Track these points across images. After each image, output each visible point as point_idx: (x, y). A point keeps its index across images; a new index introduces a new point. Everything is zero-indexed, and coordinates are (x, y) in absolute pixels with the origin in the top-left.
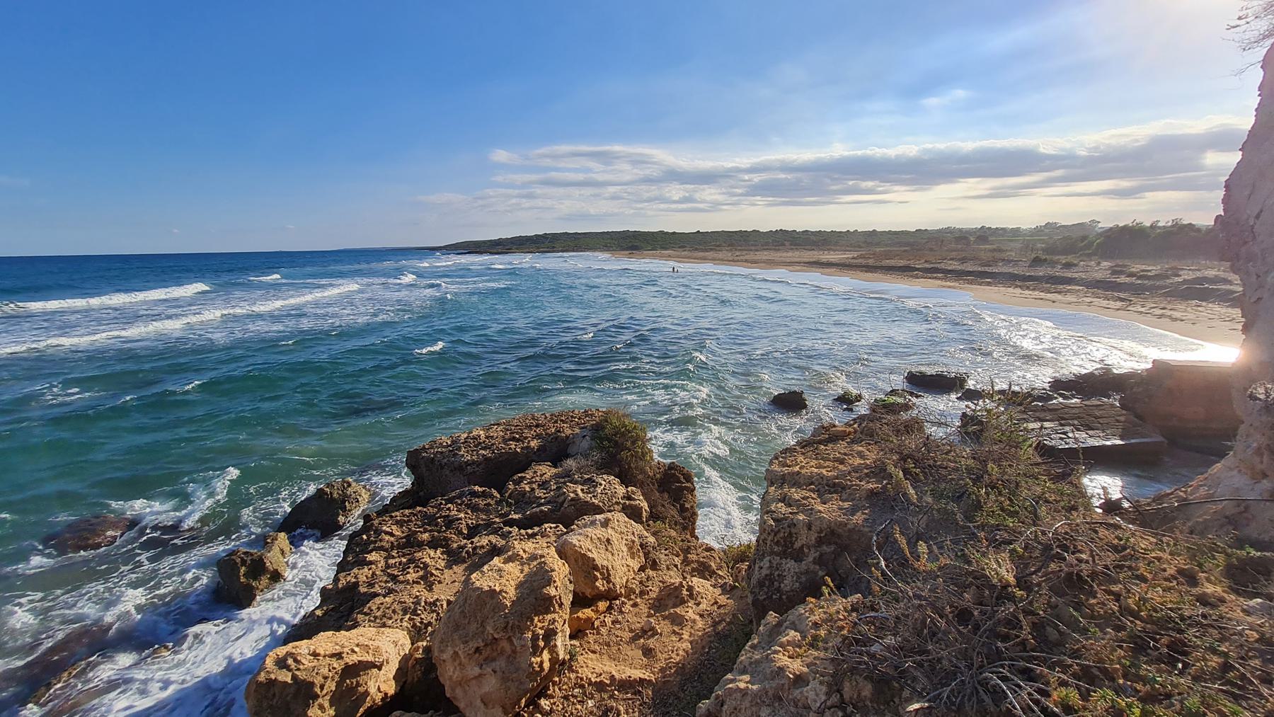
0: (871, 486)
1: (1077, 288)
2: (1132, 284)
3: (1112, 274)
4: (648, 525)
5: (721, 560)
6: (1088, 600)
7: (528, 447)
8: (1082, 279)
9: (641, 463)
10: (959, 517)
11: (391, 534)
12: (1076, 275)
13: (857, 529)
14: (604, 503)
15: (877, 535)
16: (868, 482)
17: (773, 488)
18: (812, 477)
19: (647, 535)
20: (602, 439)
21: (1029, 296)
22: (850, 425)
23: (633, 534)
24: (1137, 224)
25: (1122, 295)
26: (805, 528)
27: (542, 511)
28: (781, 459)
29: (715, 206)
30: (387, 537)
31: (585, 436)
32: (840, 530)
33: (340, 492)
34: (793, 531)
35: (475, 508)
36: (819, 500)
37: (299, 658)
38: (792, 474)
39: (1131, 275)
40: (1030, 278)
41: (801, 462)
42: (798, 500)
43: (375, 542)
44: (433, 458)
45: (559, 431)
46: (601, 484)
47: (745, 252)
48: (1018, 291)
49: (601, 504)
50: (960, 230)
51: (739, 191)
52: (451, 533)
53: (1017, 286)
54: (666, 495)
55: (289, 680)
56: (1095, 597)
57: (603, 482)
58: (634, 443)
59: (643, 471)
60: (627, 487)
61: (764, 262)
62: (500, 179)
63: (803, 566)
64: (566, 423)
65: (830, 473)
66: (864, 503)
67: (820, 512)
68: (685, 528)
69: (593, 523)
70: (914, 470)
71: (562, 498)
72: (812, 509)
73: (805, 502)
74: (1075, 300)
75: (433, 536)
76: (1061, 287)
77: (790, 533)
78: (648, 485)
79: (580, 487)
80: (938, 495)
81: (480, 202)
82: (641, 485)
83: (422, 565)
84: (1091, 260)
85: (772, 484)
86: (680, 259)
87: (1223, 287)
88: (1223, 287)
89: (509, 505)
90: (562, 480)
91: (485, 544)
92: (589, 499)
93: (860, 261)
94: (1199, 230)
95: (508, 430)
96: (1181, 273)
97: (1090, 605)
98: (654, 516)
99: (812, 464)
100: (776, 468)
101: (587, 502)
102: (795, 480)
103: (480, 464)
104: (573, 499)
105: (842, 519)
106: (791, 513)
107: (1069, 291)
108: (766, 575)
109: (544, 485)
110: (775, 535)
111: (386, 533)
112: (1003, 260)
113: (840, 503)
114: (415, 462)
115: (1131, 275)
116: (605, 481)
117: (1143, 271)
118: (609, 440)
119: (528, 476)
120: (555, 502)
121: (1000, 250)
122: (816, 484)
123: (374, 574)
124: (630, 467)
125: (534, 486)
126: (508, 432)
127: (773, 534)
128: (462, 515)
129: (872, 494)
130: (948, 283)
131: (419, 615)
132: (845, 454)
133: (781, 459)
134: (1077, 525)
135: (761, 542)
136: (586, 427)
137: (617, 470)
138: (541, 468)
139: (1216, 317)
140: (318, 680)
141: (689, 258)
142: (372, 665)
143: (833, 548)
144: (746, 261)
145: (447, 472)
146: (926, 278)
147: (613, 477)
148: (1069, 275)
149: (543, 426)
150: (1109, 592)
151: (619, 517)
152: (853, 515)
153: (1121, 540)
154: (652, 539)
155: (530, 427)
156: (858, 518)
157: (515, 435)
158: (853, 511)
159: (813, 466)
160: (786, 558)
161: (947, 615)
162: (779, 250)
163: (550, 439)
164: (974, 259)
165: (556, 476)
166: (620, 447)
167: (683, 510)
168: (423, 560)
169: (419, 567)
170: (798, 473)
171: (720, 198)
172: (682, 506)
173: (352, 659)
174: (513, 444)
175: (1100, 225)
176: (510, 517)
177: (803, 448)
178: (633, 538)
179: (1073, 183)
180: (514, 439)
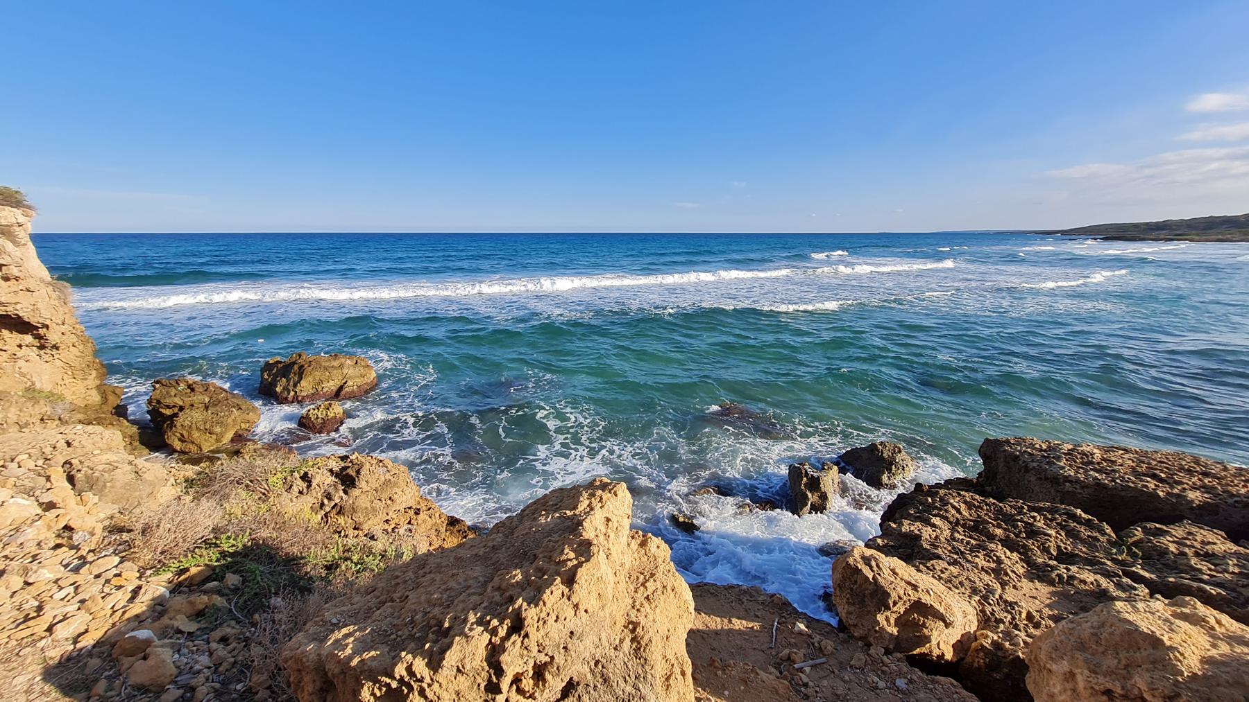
11: (958, 511)
30: (953, 512)
33: (890, 454)
35: (1071, 534)
37: (881, 565)
43: (940, 509)
44: (1018, 456)
52: (1033, 544)
55: (871, 578)
62: (1196, 135)
75: (1008, 536)
81: (1147, 172)
83: (995, 558)
89: (1134, 555)
91: (1088, 580)
103: (1087, 487)
111: (954, 507)
114: (990, 450)
123: (937, 537)
128: (1052, 532)
131: (990, 604)
140: (894, 595)
142: (942, 619)
145: (1033, 479)
168: (998, 554)
169: (991, 557)
173: (926, 599)
174: (1152, 484)
176: (1134, 569)
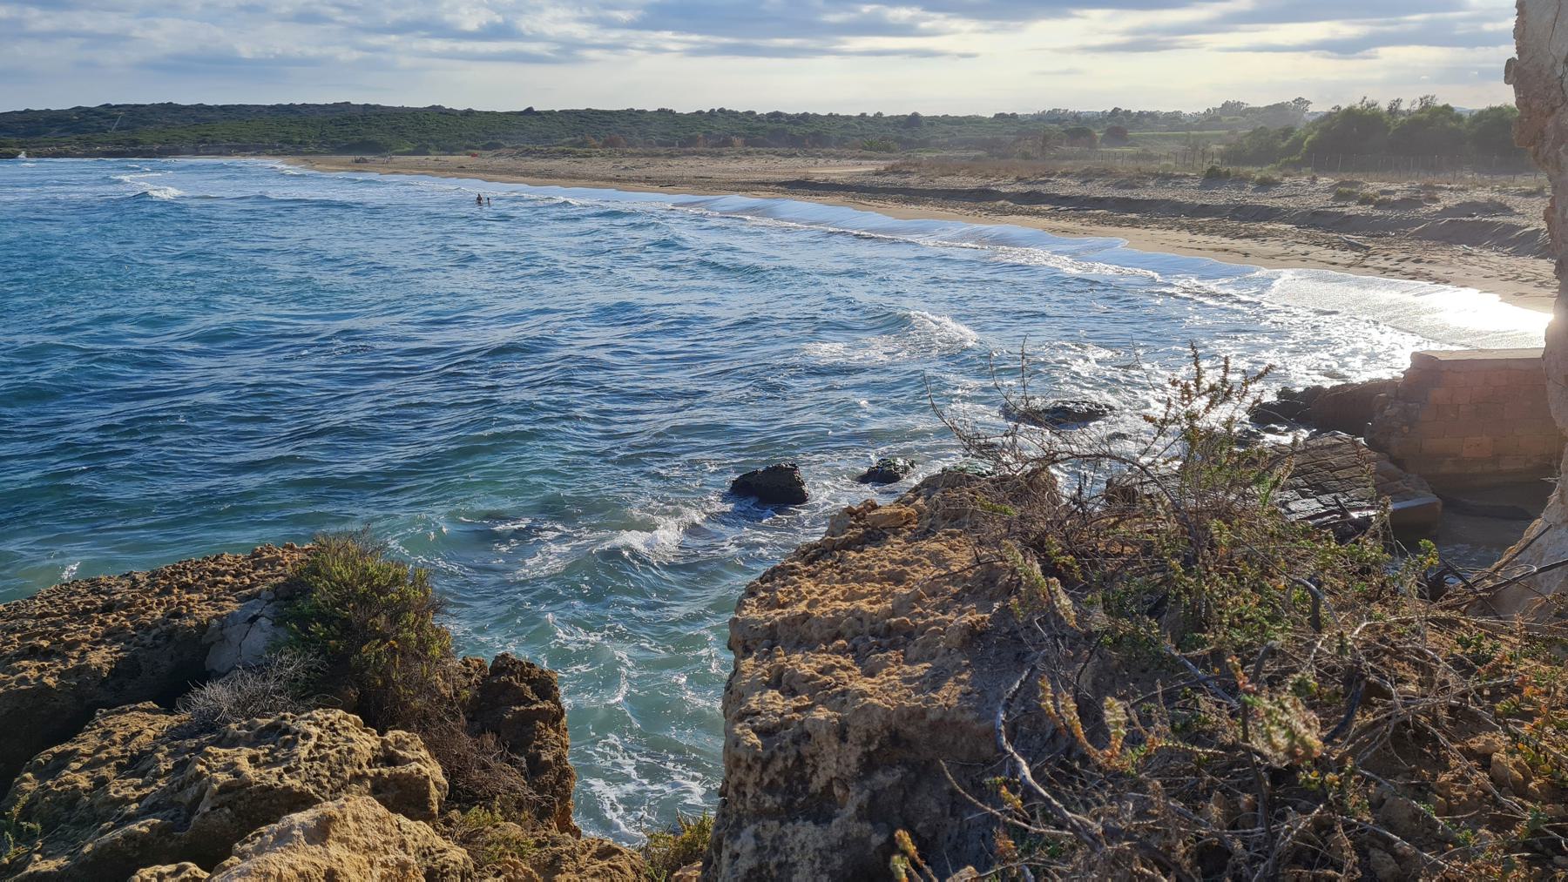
0: (967, 619)
1: (1283, 226)
2: (1368, 217)
3: (1334, 199)
4: (448, 823)
5: (638, 872)
6: (1435, 776)
7: (78, 671)
8: (1290, 210)
9: (420, 669)
10: (1168, 646)
12: (1279, 203)
13: (948, 719)
14: (319, 784)
15: (1007, 707)
16: (961, 612)
17: (750, 661)
18: (836, 621)
19: (445, 845)
20: (303, 620)
21: (1202, 246)
22: (908, 503)
23: (403, 845)
24: (1369, 106)
25: (1354, 238)
26: (833, 739)
27: (130, 837)
28: (762, 594)
29: (568, 51)
31: (254, 619)
32: (911, 729)
34: (806, 749)
36: (858, 670)
38: (793, 621)
39: (1365, 201)
40: (1204, 210)
41: (810, 592)
42: (812, 677)
45: (178, 615)
46: (307, 736)
47: (640, 163)
48: (1185, 235)
49: (311, 788)
50: (1076, 117)
51: (623, 16)
53: (1182, 227)
54: (490, 740)
56: (1446, 769)
57: (314, 730)
58: (394, 619)
59: (425, 687)
60: (382, 733)
61: (689, 183)
63: (835, 830)
64: (198, 590)
65: (876, 607)
66: (957, 660)
67: (863, 694)
68: (543, 814)
69: (284, 838)
70: (1062, 559)
71: (192, 791)
72: (844, 693)
73: (827, 678)
74: (1280, 250)
76: (1257, 226)
77: (800, 759)
78: (441, 720)
79: (247, 752)
80: (1115, 609)
82: (420, 723)
84: (1301, 174)
85: (747, 651)
86: (486, 172)
87: (1501, 219)
88: (1501, 219)
89: (25, 837)
90: (194, 742)
92: (274, 780)
93: (891, 179)
94: (1459, 118)
95: (13, 630)
96: (1439, 195)
97: (1442, 786)
98: (461, 795)
99: (834, 592)
100: (753, 613)
101: (270, 788)
102: (799, 635)
104: (226, 789)
105: (916, 701)
106: (797, 710)
107: (1269, 233)
108: (751, 871)
109: (135, 764)
110: (764, 768)
112: (1156, 175)
113: (906, 668)
115: (1365, 201)
116: (318, 724)
117: (1384, 192)
118: (326, 619)
119: (83, 749)
120: (172, 804)
121: (1150, 158)
122: (849, 633)
124: (388, 682)
125: (104, 771)
126: (15, 637)
127: (758, 767)
129: (973, 635)
130: (1063, 224)
132: (905, 562)
133: (762, 594)
134: (1388, 628)
135: (731, 792)
136: (257, 595)
137: (353, 693)
138: (123, 719)
139: (1494, 273)
141: (510, 172)
143: (898, 773)
144: (648, 180)
146: (1019, 214)
147: (340, 713)
148: (1268, 203)
149: (126, 607)
150: (1469, 754)
151: (361, 806)
152: (936, 689)
153: (1467, 644)
154: (457, 854)
155: (85, 615)
156: (949, 694)
157: (36, 641)
158: (935, 681)
159: (836, 598)
160: (794, 821)
161: (1177, 864)
162: (720, 155)
163: (148, 640)
164: (1104, 173)
165: (174, 734)
166: (355, 633)
167: (536, 768)
170: (806, 617)
171: (581, 31)
172: (534, 761)
174: (31, 670)
175: (1311, 109)
176: (31, 869)
177: (810, 562)
178: (403, 856)
179: (1272, 26)
180: (33, 653)
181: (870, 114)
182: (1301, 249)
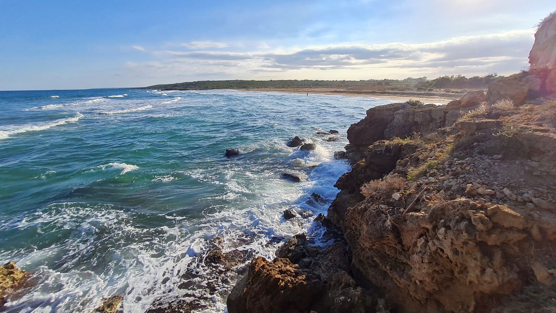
8: (438, 94)
50: (380, 81)
175: (427, 79)
181: (335, 80)
182: (443, 100)
